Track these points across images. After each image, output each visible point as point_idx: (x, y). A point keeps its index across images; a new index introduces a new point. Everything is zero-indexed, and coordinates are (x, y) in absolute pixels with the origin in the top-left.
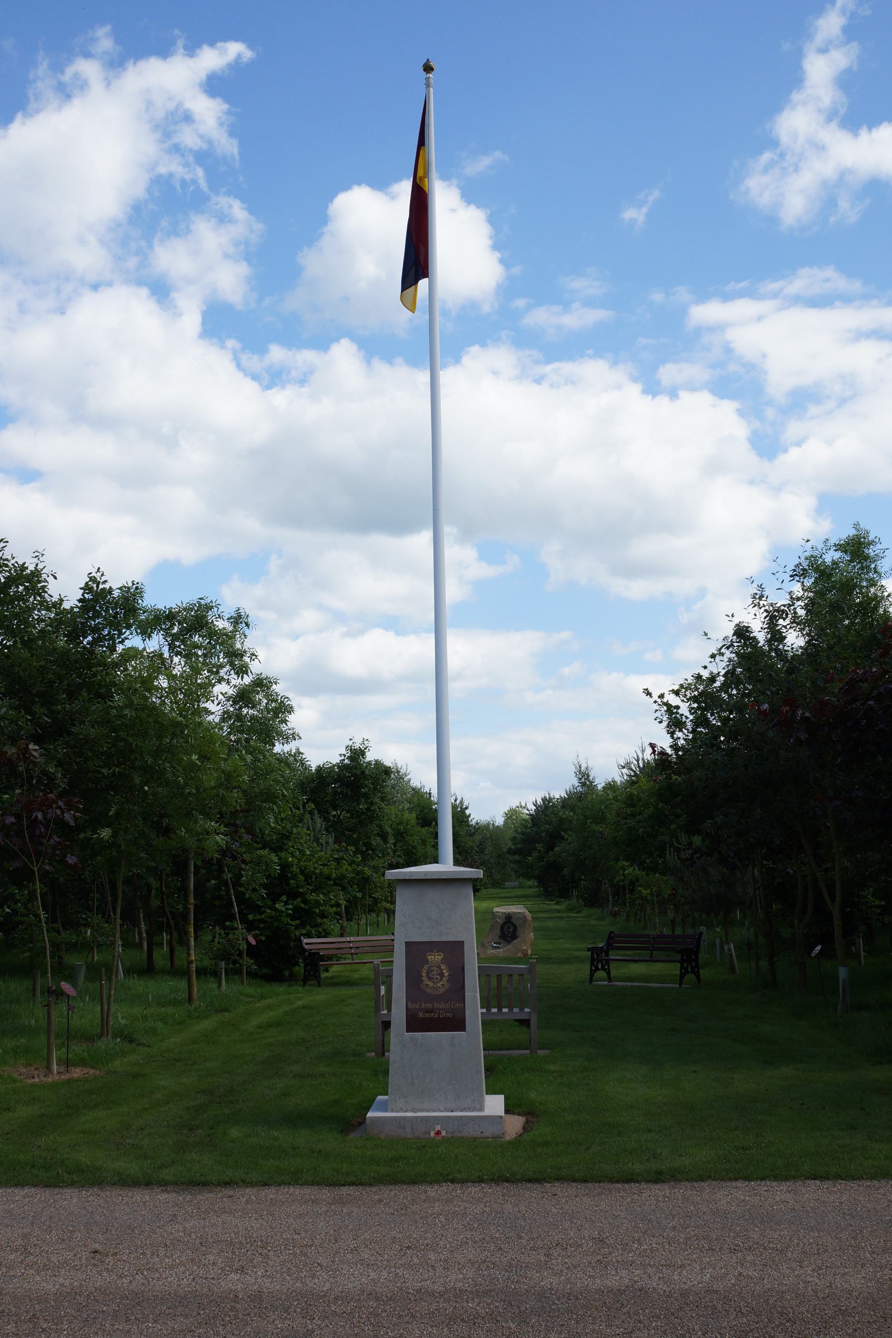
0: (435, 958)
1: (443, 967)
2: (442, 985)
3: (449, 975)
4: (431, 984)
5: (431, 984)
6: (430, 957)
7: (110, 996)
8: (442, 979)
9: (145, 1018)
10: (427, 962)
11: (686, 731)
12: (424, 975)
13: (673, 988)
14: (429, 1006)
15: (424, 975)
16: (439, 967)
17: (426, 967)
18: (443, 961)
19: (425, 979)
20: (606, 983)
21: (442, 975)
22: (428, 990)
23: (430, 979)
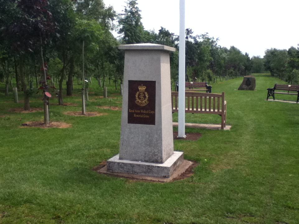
0: (142, 88)
1: (146, 93)
2: (144, 102)
3: (148, 97)
4: (140, 101)
5: (140, 101)
6: (140, 88)
7: (117, 172)
8: (145, 99)
9: (289, 118)
10: (138, 90)
11: (57, 80)
12: (137, 96)
13: (293, 104)
14: (139, 111)
15: (137, 96)
16: (144, 93)
17: (138, 93)
18: (146, 90)
19: (137, 98)
20: (272, 100)
21: (145, 97)
22: (138, 104)
23: (139, 98)
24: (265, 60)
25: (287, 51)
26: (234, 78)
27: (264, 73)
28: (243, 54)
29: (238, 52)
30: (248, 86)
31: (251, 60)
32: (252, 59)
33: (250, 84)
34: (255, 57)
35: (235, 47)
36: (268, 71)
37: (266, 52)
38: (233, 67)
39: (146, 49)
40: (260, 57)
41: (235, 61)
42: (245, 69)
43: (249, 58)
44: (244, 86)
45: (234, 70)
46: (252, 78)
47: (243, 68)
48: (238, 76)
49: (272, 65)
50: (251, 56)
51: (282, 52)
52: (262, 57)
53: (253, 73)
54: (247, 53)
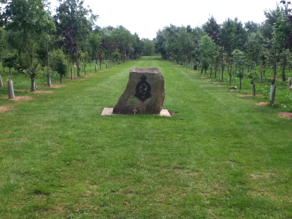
24: (157, 41)
25: (186, 28)
26: (120, 64)
27: (155, 56)
28: (132, 34)
29: (127, 33)
30: (143, 100)
31: (141, 41)
32: (142, 39)
33: (148, 95)
34: (145, 39)
35: (124, 26)
36: (158, 54)
37: (158, 31)
38: (118, 48)
39: (155, 60)
40: (150, 39)
41: (122, 40)
42: (135, 51)
43: (139, 38)
44: (135, 101)
45: (120, 52)
46: (154, 74)
47: (133, 49)
48: (127, 60)
49: (166, 45)
50: (141, 37)
51: (178, 30)
52: (151, 39)
53: (143, 56)
54: (137, 33)
